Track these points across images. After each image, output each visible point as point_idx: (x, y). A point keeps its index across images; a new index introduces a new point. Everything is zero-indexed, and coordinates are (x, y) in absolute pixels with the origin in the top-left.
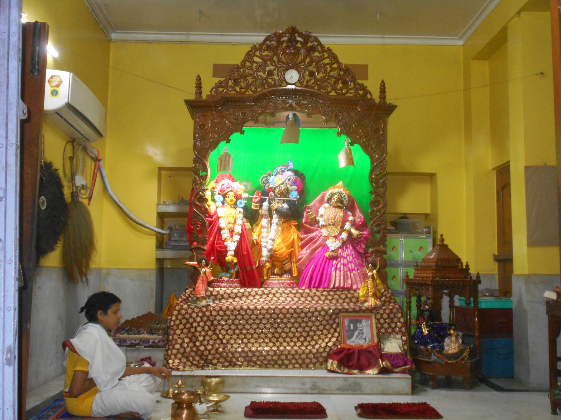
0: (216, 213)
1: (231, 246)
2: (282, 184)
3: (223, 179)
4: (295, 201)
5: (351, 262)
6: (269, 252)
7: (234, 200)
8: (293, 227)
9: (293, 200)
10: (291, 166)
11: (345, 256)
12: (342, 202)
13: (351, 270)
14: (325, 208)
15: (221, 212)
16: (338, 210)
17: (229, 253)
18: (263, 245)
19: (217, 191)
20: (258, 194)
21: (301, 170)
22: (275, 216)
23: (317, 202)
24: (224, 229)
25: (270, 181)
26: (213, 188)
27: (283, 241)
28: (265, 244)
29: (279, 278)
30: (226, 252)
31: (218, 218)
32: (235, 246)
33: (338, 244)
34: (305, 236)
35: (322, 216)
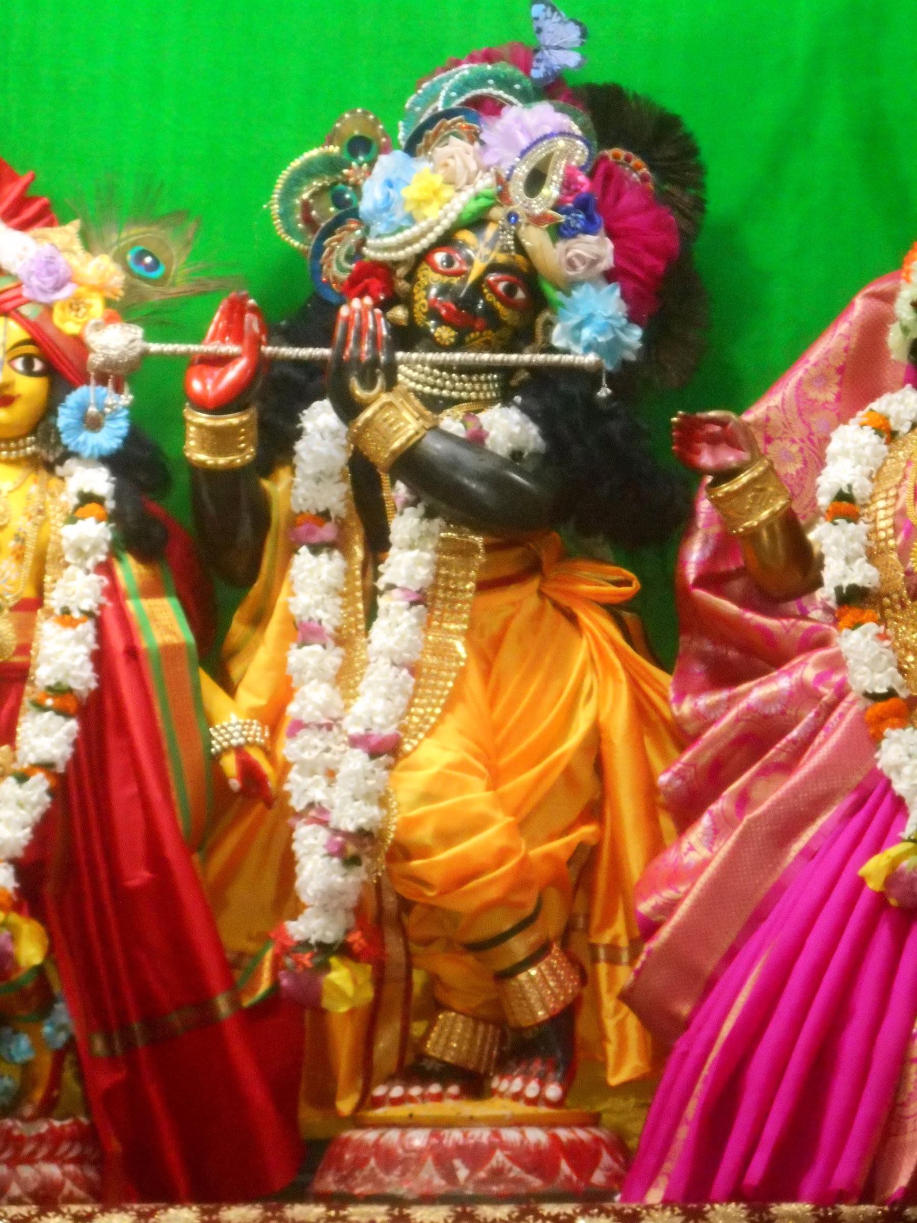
2: (478, 223)
6: (351, 862)
8: (599, 626)
10: (564, 54)
14: (889, 435)
18: (297, 803)
21: (638, 78)
22: (405, 525)
23: (821, 379)
25: (365, 206)
27: (492, 758)
28: (318, 794)
29: (450, 1108)
32: (33, 814)
34: (705, 700)
35: (846, 505)
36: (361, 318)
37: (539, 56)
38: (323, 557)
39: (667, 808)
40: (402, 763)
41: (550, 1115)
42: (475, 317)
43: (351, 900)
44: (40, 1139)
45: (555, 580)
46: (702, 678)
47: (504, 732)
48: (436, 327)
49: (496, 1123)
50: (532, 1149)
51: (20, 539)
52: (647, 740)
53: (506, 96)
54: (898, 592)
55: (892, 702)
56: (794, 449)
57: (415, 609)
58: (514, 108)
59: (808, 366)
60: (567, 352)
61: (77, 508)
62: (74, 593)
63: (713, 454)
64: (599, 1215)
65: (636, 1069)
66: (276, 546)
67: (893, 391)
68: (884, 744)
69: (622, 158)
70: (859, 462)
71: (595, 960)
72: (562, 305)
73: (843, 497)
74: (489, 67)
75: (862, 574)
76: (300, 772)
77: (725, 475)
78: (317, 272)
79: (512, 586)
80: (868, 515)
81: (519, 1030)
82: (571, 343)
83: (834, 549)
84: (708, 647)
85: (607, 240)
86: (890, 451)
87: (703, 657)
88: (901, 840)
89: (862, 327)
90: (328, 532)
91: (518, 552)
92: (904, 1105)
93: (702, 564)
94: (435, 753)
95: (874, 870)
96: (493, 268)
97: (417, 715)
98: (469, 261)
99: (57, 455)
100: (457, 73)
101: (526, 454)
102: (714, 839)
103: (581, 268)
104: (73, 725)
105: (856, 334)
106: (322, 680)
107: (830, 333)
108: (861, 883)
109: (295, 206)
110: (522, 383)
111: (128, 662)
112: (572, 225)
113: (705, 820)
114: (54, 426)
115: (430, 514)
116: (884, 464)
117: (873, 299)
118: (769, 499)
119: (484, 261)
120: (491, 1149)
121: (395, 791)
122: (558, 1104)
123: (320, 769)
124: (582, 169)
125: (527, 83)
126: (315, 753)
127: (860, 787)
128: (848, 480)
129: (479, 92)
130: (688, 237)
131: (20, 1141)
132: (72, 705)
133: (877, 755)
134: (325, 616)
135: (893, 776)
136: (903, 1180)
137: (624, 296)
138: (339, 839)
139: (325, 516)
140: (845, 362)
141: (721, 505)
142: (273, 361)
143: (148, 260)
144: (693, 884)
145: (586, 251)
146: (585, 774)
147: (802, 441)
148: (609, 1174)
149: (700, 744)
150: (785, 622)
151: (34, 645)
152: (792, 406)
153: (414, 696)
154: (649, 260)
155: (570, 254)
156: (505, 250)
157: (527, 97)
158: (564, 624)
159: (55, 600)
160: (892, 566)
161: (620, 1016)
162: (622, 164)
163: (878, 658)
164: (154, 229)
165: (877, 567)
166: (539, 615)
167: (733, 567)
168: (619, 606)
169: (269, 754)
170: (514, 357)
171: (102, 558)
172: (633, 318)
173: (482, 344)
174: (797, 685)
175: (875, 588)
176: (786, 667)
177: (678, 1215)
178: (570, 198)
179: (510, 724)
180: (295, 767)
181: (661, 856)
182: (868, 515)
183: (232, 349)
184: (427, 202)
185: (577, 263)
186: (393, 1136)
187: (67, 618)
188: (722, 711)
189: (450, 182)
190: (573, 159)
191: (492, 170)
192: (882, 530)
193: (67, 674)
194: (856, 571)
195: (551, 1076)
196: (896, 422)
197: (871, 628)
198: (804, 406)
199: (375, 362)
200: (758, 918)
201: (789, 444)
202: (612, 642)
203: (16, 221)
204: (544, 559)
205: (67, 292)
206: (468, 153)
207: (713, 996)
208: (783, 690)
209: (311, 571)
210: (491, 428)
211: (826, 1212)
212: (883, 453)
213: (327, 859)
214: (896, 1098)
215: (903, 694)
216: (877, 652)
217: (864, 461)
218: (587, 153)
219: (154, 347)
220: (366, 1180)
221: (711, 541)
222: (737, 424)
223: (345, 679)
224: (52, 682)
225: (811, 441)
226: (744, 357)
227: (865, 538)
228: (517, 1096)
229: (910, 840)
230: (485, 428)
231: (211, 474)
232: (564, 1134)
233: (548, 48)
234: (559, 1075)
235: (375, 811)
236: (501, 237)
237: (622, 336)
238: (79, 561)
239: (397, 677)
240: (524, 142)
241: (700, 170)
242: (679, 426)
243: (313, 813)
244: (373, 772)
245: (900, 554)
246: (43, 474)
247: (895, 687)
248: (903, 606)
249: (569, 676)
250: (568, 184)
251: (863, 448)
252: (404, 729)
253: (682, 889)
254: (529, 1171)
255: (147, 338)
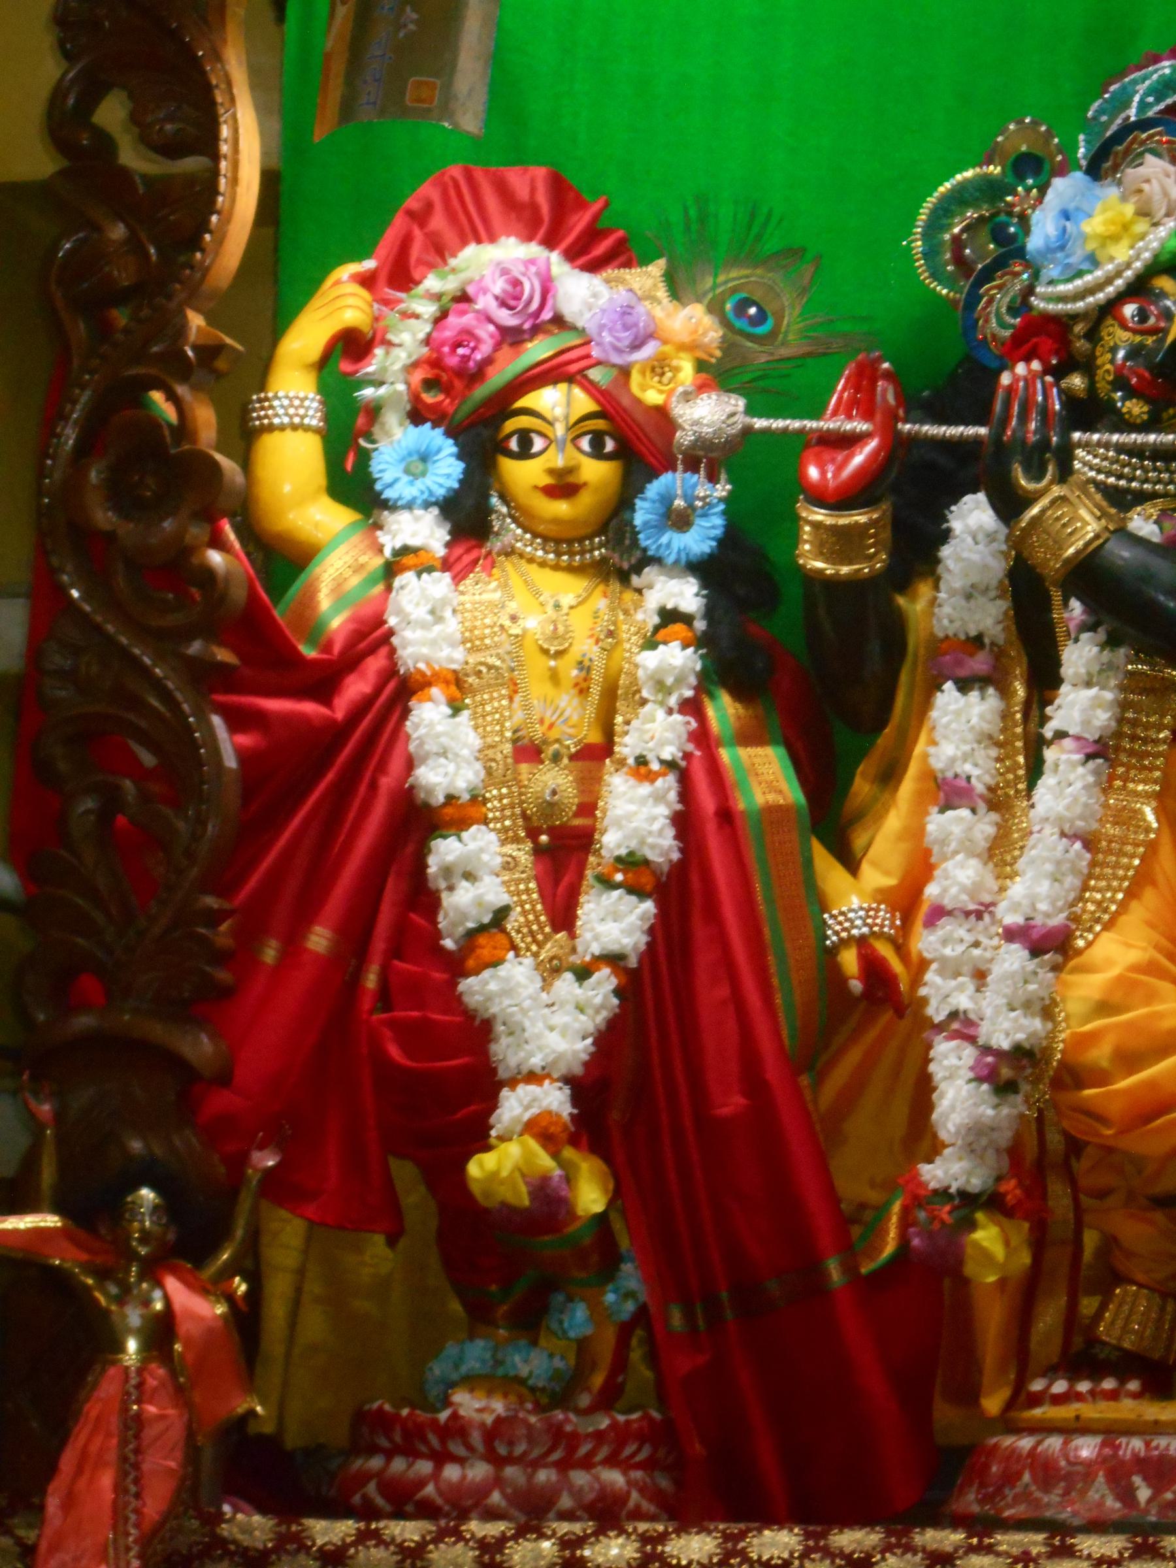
0: (372, 635)
1: (545, 1017)
3: (479, 231)
6: (1004, 1089)
7: (597, 472)
15: (431, 621)
17: (514, 1106)
18: (936, 1012)
19: (392, 370)
20: (862, 402)
22: (1079, 656)
24: (455, 816)
25: (1034, 243)
26: (353, 345)
30: (485, 1085)
31: (402, 690)
36: (1026, 388)
38: (974, 695)
40: (1072, 964)
43: (1004, 1138)
44: (599, 1436)
48: (1124, 399)
51: (584, 667)
57: (1091, 765)
61: (657, 629)
62: (652, 738)
66: (912, 685)
76: (941, 972)
78: (970, 326)
90: (979, 663)
94: (1114, 952)
97: (1094, 902)
99: (633, 561)
100: (1156, 71)
104: (648, 906)
106: (972, 854)
109: (943, 242)
111: (720, 826)
114: (630, 523)
115: (1112, 642)
121: (1063, 1000)
123: (966, 969)
126: (960, 949)
131: (573, 1440)
132: (647, 881)
134: (975, 772)
138: (990, 1059)
139: (977, 641)
142: (913, 440)
143: (753, 311)
151: (601, 804)
153: (1090, 876)
159: (628, 746)
164: (759, 271)
169: (901, 949)
171: (689, 693)
180: (934, 966)
183: (862, 426)
184: (1115, 238)
186: (1054, 1443)
187: (643, 770)
189: (1144, 212)
193: (642, 842)
199: (1044, 445)
203: (582, 260)
205: (649, 350)
209: (957, 713)
213: (973, 1084)
219: (760, 423)
220: (1017, 1500)
223: (1001, 853)
224: (623, 852)
231: (831, 585)
235: (1037, 1024)
238: (660, 697)
239: (1067, 851)
243: (955, 1026)
244: (1035, 973)
246: (615, 586)
252: (1075, 918)
255: (750, 411)
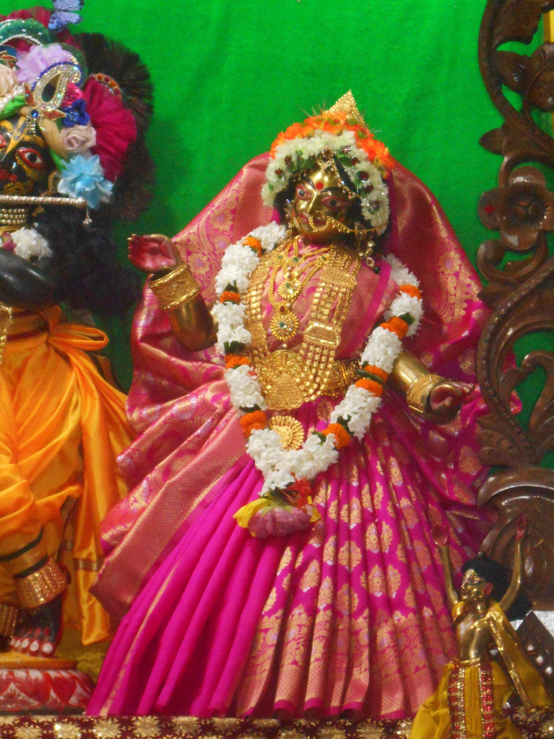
2: (14, 116)
4: (80, 211)
5: (383, 560)
8: (84, 363)
9: (70, 208)
11: (355, 521)
12: (352, 212)
13: (377, 608)
16: (326, 258)
21: (113, 32)
23: (222, 217)
33: (316, 453)
34: (146, 411)
35: (233, 293)
37: (54, 15)
39: (122, 476)
41: (45, 662)
42: (11, 173)
45: (58, 335)
46: (146, 397)
47: (22, 428)
49: (12, 667)
50: (33, 683)
52: (112, 435)
53: (33, 39)
54: (262, 347)
55: (257, 413)
56: (205, 259)
58: (38, 47)
59: (214, 209)
60: (67, 196)
63: (153, 261)
64: (68, 722)
65: (99, 636)
67: (264, 225)
68: (251, 438)
69: (103, 79)
70: (241, 267)
71: (77, 568)
72: (64, 168)
73: (231, 288)
74: (23, 21)
75: (241, 335)
77: (162, 273)
79: (31, 338)
80: (246, 299)
81: (28, 610)
82: (69, 191)
83: (224, 319)
84: (150, 378)
85: (92, 128)
86: (260, 261)
87: (146, 384)
88: (259, 497)
89: (247, 185)
91: (34, 317)
92: (255, 658)
93: (146, 327)
95: (243, 515)
96: (22, 144)
98: (8, 140)
100: (4, 24)
101: (40, 258)
102: (149, 495)
103: (76, 145)
105: (243, 190)
107: (228, 189)
108: (235, 522)
110: (39, 215)
112: (71, 119)
113: (144, 484)
116: (257, 269)
117: (254, 169)
118: (186, 289)
119: (16, 140)
120: (7, 683)
122: (50, 655)
124: (78, 85)
125: (46, 32)
127: (236, 464)
128: (234, 278)
129: (16, 36)
130: (142, 129)
133: (247, 445)
135: (256, 458)
136: (253, 703)
137: (102, 163)
140: (236, 207)
141: (158, 292)
144: (135, 522)
145: (79, 135)
146: (73, 454)
147: (209, 254)
148: (80, 698)
149: (143, 437)
150: (195, 364)
152: (203, 233)
154: (117, 141)
155: (69, 137)
156: (30, 133)
157: (46, 41)
158: (62, 363)
160: (259, 331)
161: (91, 603)
162: (103, 83)
163: (249, 387)
165: (250, 331)
166: (46, 356)
167: (165, 330)
168: (95, 352)
170: (33, 198)
172: (108, 176)
173: (14, 190)
174: (201, 402)
175: (248, 344)
176: (195, 392)
177: (116, 723)
178: (69, 103)
179: (26, 423)
181: (117, 505)
182: (246, 299)
185: (74, 142)
188: (157, 417)
190: (73, 79)
191: (23, 84)
192: (253, 309)
194: (237, 333)
195: (46, 638)
196: (265, 244)
197: (245, 368)
198: (211, 233)
200: (174, 542)
201: (201, 256)
202: (91, 374)
204: (51, 323)
206: (9, 74)
207: (145, 590)
208: (193, 405)
210: (18, 242)
211: (206, 722)
212: (256, 262)
214: (250, 654)
215: (263, 408)
216: (248, 383)
217: (244, 267)
218: (80, 75)
221: (152, 314)
222: (168, 243)
225: (214, 254)
226: (177, 202)
227: (243, 313)
228: (25, 650)
229: (264, 497)
230: (15, 241)
232: (53, 674)
233: (59, 11)
234: (51, 638)
236: (27, 125)
237: (100, 187)
240: (43, 67)
241: (150, 88)
242: (132, 243)
245: (264, 323)
247: (258, 404)
248: (265, 355)
249: (63, 395)
250: (69, 93)
251: (244, 259)
253: (129, 525)
254: (31, 696)
